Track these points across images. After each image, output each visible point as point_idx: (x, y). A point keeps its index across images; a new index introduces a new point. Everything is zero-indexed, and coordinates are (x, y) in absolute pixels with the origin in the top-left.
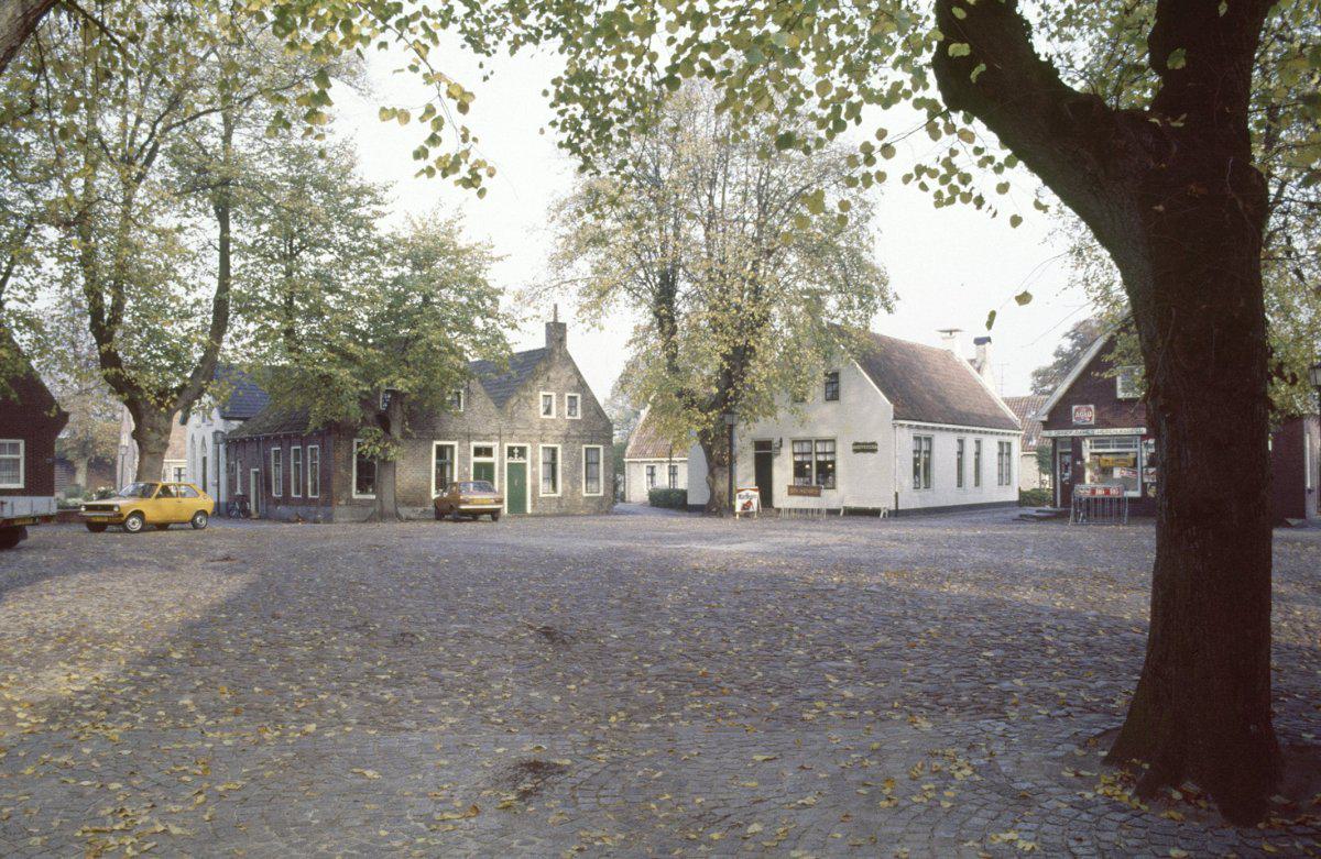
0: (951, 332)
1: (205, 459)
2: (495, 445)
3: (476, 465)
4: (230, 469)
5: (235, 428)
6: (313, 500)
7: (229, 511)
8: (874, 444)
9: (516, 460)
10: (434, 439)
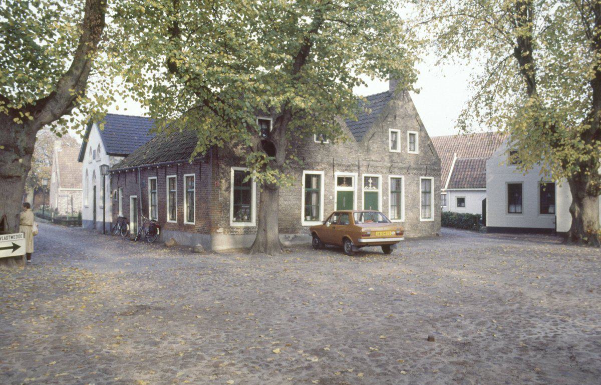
1: (95, 187)
2: (354, 175)
3: (339, 193)
4: (115, 197)
5: (117, 162)
6: (188, 227)
7: (113, 230)
9: (371, 189)
10: (304, 169)
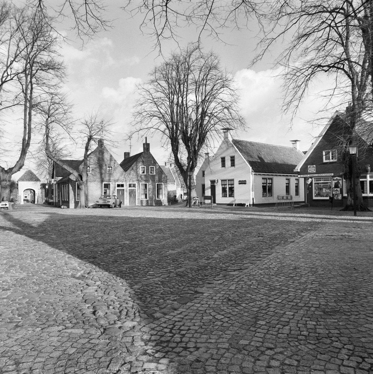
0: (296, 141)
3: (117, 190)
8: (245, 181)
9: (132, 188)
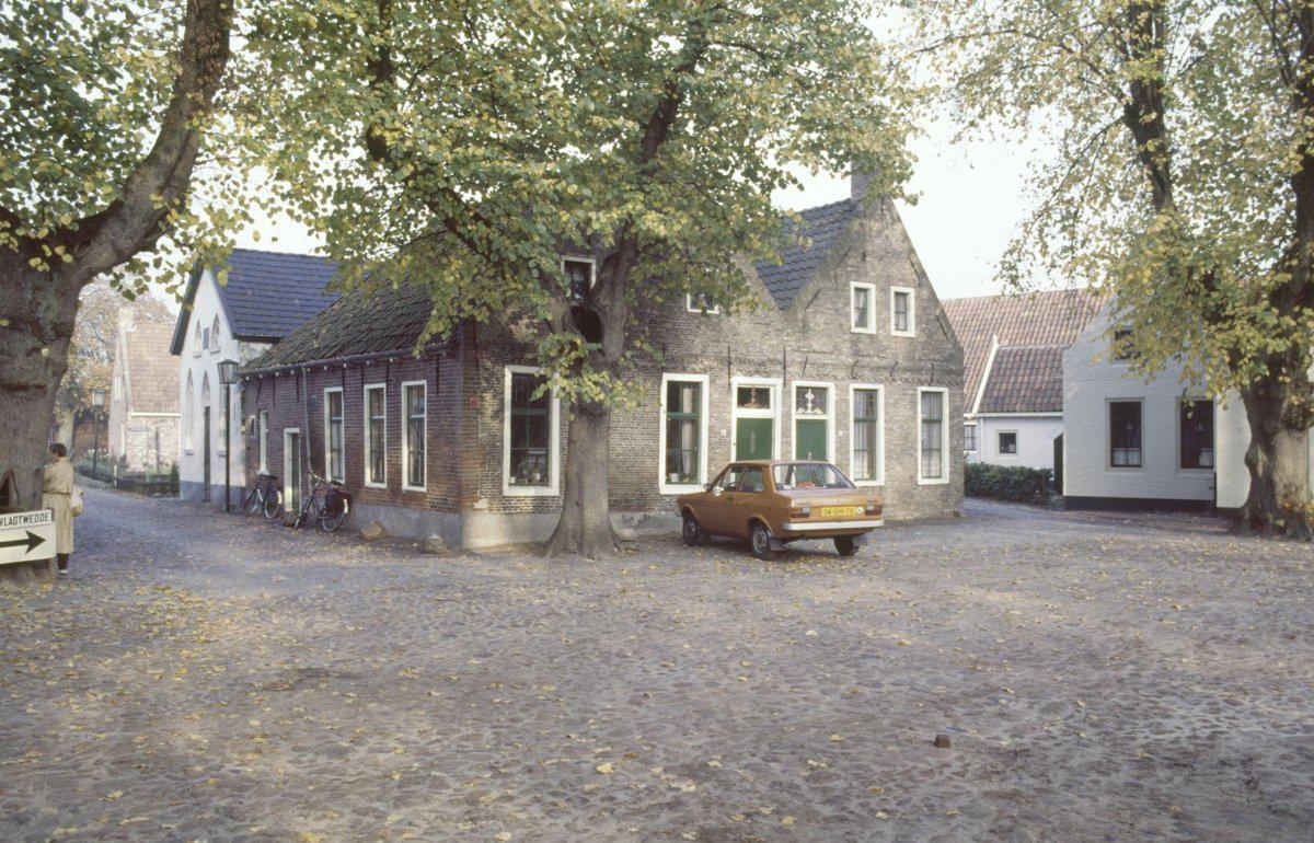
1: (207, 410)
2: (774, 384)
3: (742, 422)
4: (252, 430)
5: (256, 355)
6: (412, 496)
7: (246, 503)
9: (811, 415)
10: (664, 370)
